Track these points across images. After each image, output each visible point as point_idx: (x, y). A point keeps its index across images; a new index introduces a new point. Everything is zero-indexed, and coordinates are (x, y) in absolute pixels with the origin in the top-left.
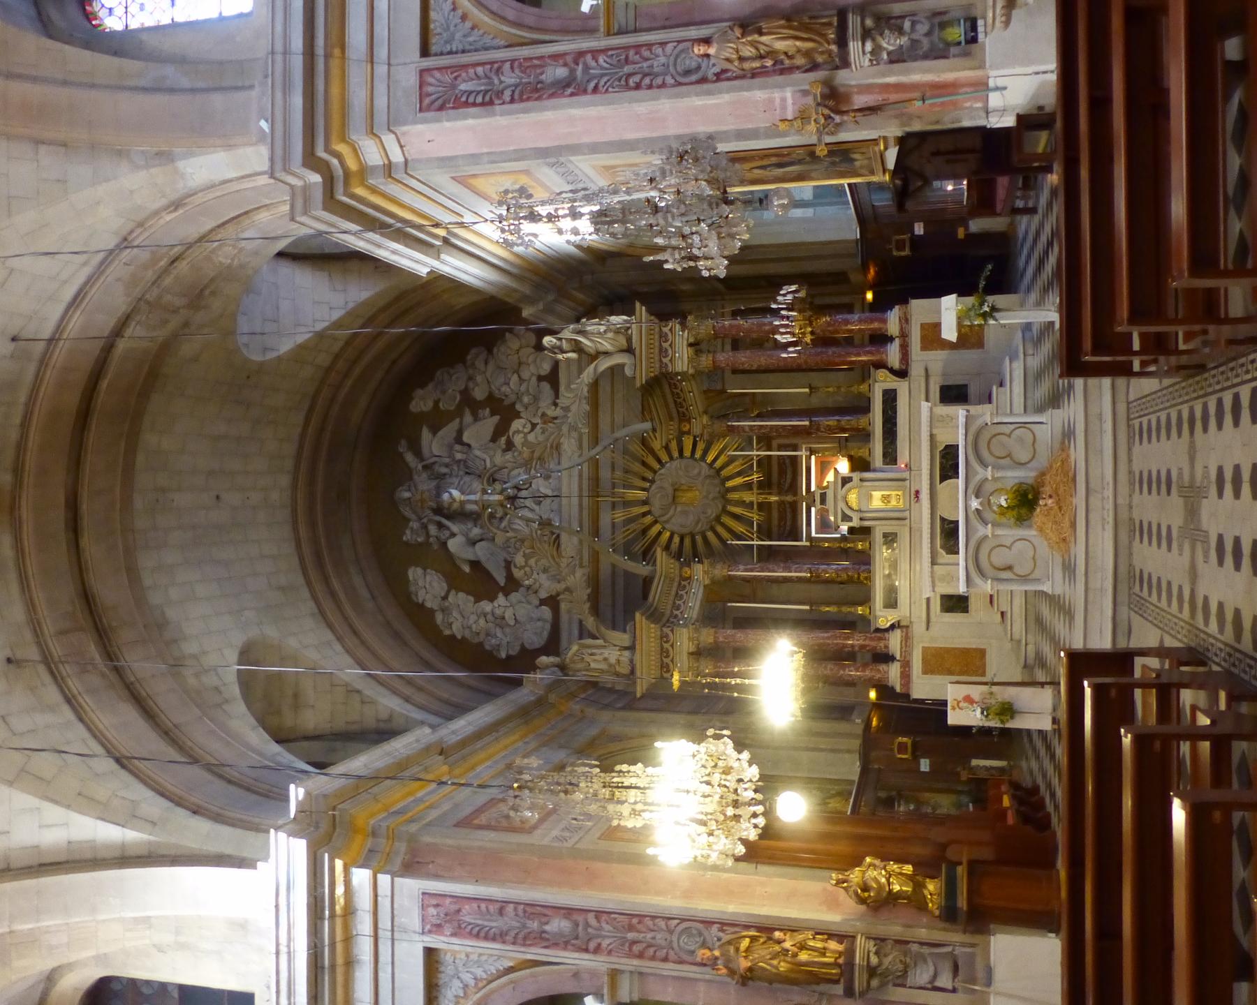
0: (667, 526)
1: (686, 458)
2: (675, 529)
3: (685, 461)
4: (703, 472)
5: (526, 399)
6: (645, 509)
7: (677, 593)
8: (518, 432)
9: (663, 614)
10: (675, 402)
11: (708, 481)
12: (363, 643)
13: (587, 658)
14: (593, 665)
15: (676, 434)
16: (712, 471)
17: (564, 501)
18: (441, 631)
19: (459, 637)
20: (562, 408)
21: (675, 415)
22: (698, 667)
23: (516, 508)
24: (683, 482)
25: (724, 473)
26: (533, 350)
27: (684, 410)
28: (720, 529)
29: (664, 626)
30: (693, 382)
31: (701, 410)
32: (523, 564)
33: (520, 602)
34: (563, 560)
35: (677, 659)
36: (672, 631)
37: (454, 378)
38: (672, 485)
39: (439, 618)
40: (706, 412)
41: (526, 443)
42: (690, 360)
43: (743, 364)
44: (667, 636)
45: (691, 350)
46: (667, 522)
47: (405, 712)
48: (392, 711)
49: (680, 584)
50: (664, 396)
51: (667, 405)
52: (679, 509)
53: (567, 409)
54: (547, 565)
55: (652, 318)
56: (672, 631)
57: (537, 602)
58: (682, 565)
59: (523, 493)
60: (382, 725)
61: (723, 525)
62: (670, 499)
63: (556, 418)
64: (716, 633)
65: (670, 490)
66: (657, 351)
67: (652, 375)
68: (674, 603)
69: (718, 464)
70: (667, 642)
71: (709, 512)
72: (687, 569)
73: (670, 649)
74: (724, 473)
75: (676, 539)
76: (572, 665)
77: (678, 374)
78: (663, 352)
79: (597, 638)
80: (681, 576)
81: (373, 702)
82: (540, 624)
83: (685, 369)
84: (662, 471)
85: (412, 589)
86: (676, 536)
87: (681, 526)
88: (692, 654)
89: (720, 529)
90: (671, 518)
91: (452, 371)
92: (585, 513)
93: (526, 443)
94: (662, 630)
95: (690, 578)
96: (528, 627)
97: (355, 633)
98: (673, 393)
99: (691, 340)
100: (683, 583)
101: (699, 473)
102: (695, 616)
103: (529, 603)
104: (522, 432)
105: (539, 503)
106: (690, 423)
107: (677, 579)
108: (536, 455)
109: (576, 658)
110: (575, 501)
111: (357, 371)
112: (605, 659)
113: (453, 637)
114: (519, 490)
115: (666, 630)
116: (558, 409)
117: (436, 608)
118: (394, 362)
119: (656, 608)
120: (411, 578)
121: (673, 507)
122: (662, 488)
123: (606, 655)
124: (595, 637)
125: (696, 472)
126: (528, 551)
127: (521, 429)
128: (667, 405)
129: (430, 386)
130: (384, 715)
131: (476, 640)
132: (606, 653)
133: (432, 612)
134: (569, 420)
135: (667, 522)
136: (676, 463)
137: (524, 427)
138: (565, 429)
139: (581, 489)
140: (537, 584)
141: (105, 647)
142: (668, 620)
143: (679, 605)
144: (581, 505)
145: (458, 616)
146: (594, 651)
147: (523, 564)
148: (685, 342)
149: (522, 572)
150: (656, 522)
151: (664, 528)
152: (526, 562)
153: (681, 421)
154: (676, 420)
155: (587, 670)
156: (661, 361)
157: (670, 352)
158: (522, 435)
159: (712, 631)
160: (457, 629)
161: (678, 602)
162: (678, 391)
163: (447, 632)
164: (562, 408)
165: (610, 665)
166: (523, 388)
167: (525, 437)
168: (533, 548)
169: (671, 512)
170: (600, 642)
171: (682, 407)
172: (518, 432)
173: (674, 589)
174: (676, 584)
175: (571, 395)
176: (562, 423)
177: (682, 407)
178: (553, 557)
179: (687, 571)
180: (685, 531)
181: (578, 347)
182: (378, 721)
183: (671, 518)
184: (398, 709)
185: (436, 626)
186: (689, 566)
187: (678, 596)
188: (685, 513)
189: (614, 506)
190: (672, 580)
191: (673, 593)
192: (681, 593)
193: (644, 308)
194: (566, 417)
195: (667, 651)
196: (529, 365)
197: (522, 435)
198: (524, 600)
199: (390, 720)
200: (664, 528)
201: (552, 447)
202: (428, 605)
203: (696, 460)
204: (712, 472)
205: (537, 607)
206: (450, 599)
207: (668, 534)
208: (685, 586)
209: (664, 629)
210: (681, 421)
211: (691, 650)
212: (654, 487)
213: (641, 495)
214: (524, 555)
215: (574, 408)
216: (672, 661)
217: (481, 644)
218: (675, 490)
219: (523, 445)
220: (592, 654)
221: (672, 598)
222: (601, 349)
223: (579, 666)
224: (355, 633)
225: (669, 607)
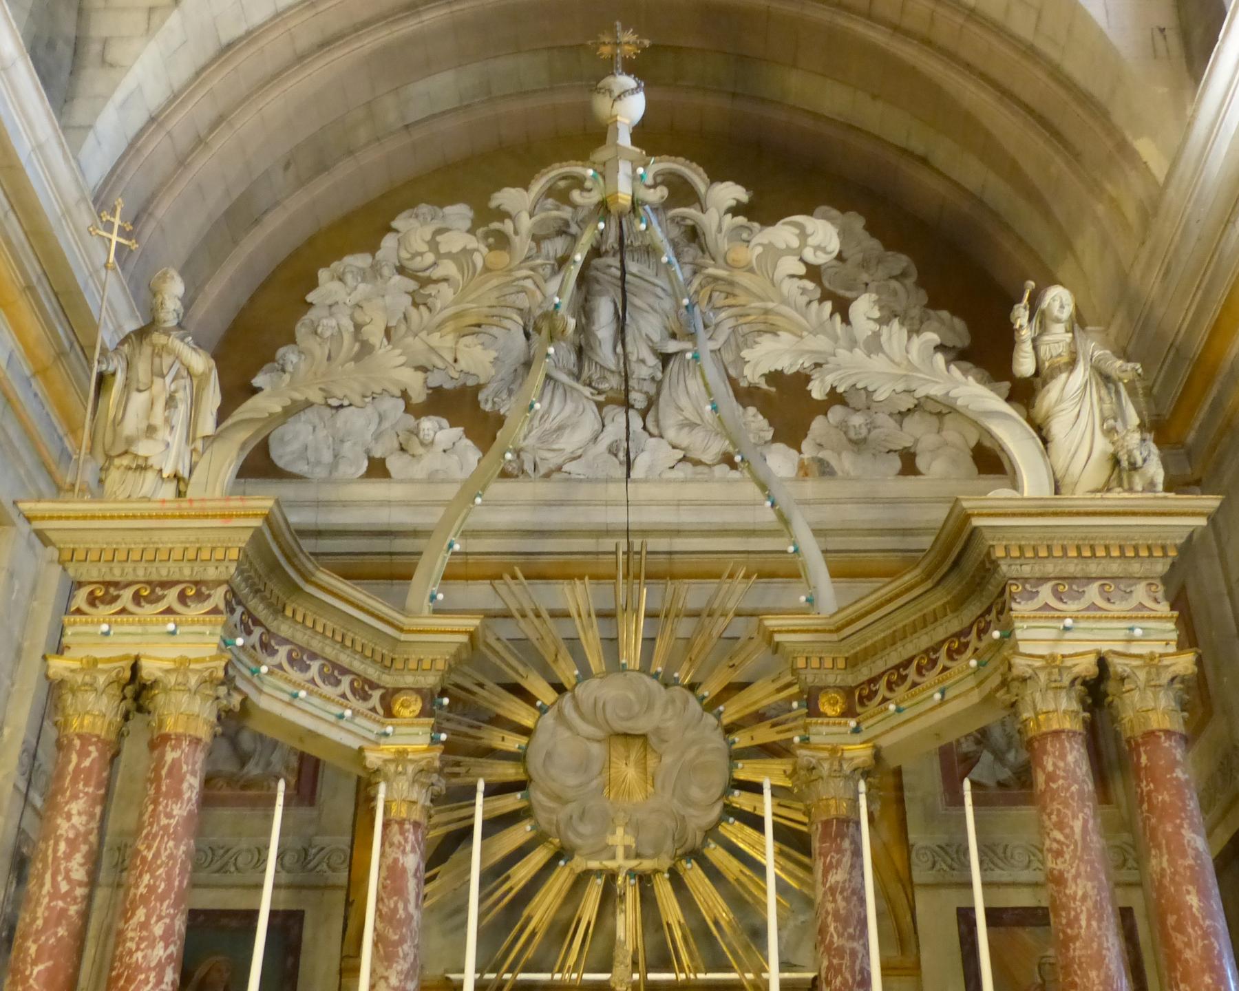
0: (549, 718)
1: (732, 768)
2: (541, 738)
3: (723, 762)
4: (691, 811)
5: (857, 420)
6: (595, 662)
7: (345, 671)
8: (803, 235)
9: (279, 610)
10: (906, 664)
11: (670, 824)
12: (301, 58)
13: (161, 388)
14: (138, 401)
15: (810, 678)
16: (699, 836)
17: (616, 491)
18: (327, 265)
19: (310, 298)
20: (876, 335)
21: (865, 673)
22: (92, 686)
23: (600, 405)
24: (668, 760)
25: (694, 875)
26: (973, 443)
27: (883, 691)
28: (539, 857)
29: (233, 592)
30: (975, 697)
31: (885, 742)
32: (443, 249)
33: (381, 418)
34: (449, 340)
35: (126, 627)
36: (215, 611)
37: (894, 284)
38: (657, 730)
39: (360, 261)
40: (877, 756)
41: (773, 253)
42: (1050, 661)
43: (1060, 826)
44: (201, 597)
45: (1086, 666)
46: (561, 717)
47: (119, 96)
48: (127, 69)
49: (374, 686)
50: (925, 622)
51: (894, 640)
52: (596, 748)
53: (874, 345)
54: (439, 305)
55: (1172, 553)
56: (215, 611)
57: (377, 454)
58: (429, 698)
59: (636, 423)
60: (95, 48)
61: (549, 868)
62: (621, 726)
63: (846, 320)
64: (196, 741)
65: (642, 725)
66: (1072, 568)
67: (999, 553)
68: (314, 656)
69: (716, 854)
70: (182, 598)
71: (586, 829)
72: (417, 707)
73: (162, 606)
74: (694, 875)
75: (513, 743)
76: (147, 350)
77: (1008, 633)
78: (1068, 585)
79: (219, 422)
80: (397, 690)
81: (149, 31)
82: (327, 457)
83: (1024, 648)
84: (695, 706)
85: (424, 209)
86: (523, 741)
87: (549, 755)
88: (135, 668)
89: (539, 857)
90: (569, 727)
91: (910, 282)
92: (588, 544)
93: (773, 253)
94: (219, 583)
95: (389, 713)
96: (322, 433)
97: (325, 44)
98: (936, 649)
99: (1119, 666)
100: (377, 695)
101: (688, 802)
102: (264, 703)
103: (378, 436)
104: (804, 244)
105: (612, 451)
106: (844, 714)
107: (388, 680)
108: (743, 279)
109: (167, 360)
110: (617, 517)
111: (908, 52)
112: (151, 430)
113: (313, 284)
114: (644, 414)
115: (218, 597)
116: (876, 327)
117: (379, 254)
118: (924, 161)
119: (297, 589)
120: (448, 210)
121: (599, 734)
122: (650, 706)
123: (163, 434)
124: (223, 414)
125: (695, 793)
126: (478, 260)
127: (811, 241)
128: (894, 640)
129: (874, 244)
130: (116, 53)
131: (301, 331)
132: (177, 438)
133: (372, 247)
134: (842, 353)
135: (561, 717)
136: (716, 740)
137: (817, 248)
138: (820, 343)
139: (645, 533)
140: (420, 450)
141: (385, 17)
142: (257, 622)
143: (305, 668)
144: (606, 532)
145: (356, 297)
146: (182, 410)
147: (443, 249)
148: (1105, 647)
149: (424, 248)
150: (560, 688)
151: (543, 710)
152: (449, 255)
153: (848, 692)
154: (850, 680)
155: (126, 386)
156: (1043, 580)
157: (1072, 606)
158: (795, 243)
159: (204, 733)
160: (328, 288)
161: (315, 666)
162: (943, 661)
163: (323, 274)
164: (876, 335)
165: (130, 441)
166: (883, 419)
167: (789, 251)
168: (487, 269)
169: (585, 728)
170: (207, 425)
171: (890, 687)
172: (803, 235)
173: (357, 665)
174: (372, 673)
175: (914, 355)
176: (836, 339)
177: (890, 687)
178: (457, 316)
179: (409, 708)
180: (536, 761)
181: (1041, 377)
182: (105, 42)
183: (569, 727)
184: (128, 83)
185: (339, 256)
186: (423, 713)
187: (334, 672)
188: (584, 765)
189: (606, 615)
190: (387, 665)
191: (344, 659)
192: (346, 681)
193: (1202, 522)
194: (853, 343)
195: (153, 600)
196: (939, 431)
197: (795, 243)
198: (386, 425)
199: (104, 62)
200: (543, 710)
201: (767, 312)
202: (389, 242)
203: (726, 793)
204: (694, 838)
205: (368, 452)
206: (397, 278)
207: (529, 723)
208: (365, 697)
209: (222, 590)
210: (848, 692)
211: (144, 663)
212: (654, 685)
213: (632, 654)
214: (467, 252)
215: (878, 363)
216: (123, 611)
217: (292, 340)
218: (644, 736)
219: (769, 247)
220: (171, 402)
221: (330, 651)
222: (1058, 429)
223: (142, 368)
224: (325, 44)
225: (301, 637)
